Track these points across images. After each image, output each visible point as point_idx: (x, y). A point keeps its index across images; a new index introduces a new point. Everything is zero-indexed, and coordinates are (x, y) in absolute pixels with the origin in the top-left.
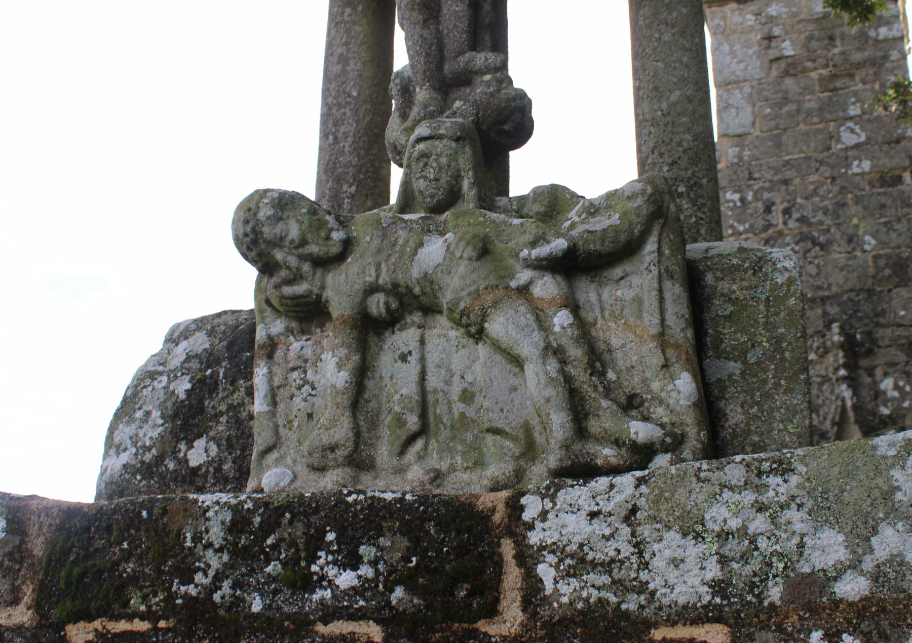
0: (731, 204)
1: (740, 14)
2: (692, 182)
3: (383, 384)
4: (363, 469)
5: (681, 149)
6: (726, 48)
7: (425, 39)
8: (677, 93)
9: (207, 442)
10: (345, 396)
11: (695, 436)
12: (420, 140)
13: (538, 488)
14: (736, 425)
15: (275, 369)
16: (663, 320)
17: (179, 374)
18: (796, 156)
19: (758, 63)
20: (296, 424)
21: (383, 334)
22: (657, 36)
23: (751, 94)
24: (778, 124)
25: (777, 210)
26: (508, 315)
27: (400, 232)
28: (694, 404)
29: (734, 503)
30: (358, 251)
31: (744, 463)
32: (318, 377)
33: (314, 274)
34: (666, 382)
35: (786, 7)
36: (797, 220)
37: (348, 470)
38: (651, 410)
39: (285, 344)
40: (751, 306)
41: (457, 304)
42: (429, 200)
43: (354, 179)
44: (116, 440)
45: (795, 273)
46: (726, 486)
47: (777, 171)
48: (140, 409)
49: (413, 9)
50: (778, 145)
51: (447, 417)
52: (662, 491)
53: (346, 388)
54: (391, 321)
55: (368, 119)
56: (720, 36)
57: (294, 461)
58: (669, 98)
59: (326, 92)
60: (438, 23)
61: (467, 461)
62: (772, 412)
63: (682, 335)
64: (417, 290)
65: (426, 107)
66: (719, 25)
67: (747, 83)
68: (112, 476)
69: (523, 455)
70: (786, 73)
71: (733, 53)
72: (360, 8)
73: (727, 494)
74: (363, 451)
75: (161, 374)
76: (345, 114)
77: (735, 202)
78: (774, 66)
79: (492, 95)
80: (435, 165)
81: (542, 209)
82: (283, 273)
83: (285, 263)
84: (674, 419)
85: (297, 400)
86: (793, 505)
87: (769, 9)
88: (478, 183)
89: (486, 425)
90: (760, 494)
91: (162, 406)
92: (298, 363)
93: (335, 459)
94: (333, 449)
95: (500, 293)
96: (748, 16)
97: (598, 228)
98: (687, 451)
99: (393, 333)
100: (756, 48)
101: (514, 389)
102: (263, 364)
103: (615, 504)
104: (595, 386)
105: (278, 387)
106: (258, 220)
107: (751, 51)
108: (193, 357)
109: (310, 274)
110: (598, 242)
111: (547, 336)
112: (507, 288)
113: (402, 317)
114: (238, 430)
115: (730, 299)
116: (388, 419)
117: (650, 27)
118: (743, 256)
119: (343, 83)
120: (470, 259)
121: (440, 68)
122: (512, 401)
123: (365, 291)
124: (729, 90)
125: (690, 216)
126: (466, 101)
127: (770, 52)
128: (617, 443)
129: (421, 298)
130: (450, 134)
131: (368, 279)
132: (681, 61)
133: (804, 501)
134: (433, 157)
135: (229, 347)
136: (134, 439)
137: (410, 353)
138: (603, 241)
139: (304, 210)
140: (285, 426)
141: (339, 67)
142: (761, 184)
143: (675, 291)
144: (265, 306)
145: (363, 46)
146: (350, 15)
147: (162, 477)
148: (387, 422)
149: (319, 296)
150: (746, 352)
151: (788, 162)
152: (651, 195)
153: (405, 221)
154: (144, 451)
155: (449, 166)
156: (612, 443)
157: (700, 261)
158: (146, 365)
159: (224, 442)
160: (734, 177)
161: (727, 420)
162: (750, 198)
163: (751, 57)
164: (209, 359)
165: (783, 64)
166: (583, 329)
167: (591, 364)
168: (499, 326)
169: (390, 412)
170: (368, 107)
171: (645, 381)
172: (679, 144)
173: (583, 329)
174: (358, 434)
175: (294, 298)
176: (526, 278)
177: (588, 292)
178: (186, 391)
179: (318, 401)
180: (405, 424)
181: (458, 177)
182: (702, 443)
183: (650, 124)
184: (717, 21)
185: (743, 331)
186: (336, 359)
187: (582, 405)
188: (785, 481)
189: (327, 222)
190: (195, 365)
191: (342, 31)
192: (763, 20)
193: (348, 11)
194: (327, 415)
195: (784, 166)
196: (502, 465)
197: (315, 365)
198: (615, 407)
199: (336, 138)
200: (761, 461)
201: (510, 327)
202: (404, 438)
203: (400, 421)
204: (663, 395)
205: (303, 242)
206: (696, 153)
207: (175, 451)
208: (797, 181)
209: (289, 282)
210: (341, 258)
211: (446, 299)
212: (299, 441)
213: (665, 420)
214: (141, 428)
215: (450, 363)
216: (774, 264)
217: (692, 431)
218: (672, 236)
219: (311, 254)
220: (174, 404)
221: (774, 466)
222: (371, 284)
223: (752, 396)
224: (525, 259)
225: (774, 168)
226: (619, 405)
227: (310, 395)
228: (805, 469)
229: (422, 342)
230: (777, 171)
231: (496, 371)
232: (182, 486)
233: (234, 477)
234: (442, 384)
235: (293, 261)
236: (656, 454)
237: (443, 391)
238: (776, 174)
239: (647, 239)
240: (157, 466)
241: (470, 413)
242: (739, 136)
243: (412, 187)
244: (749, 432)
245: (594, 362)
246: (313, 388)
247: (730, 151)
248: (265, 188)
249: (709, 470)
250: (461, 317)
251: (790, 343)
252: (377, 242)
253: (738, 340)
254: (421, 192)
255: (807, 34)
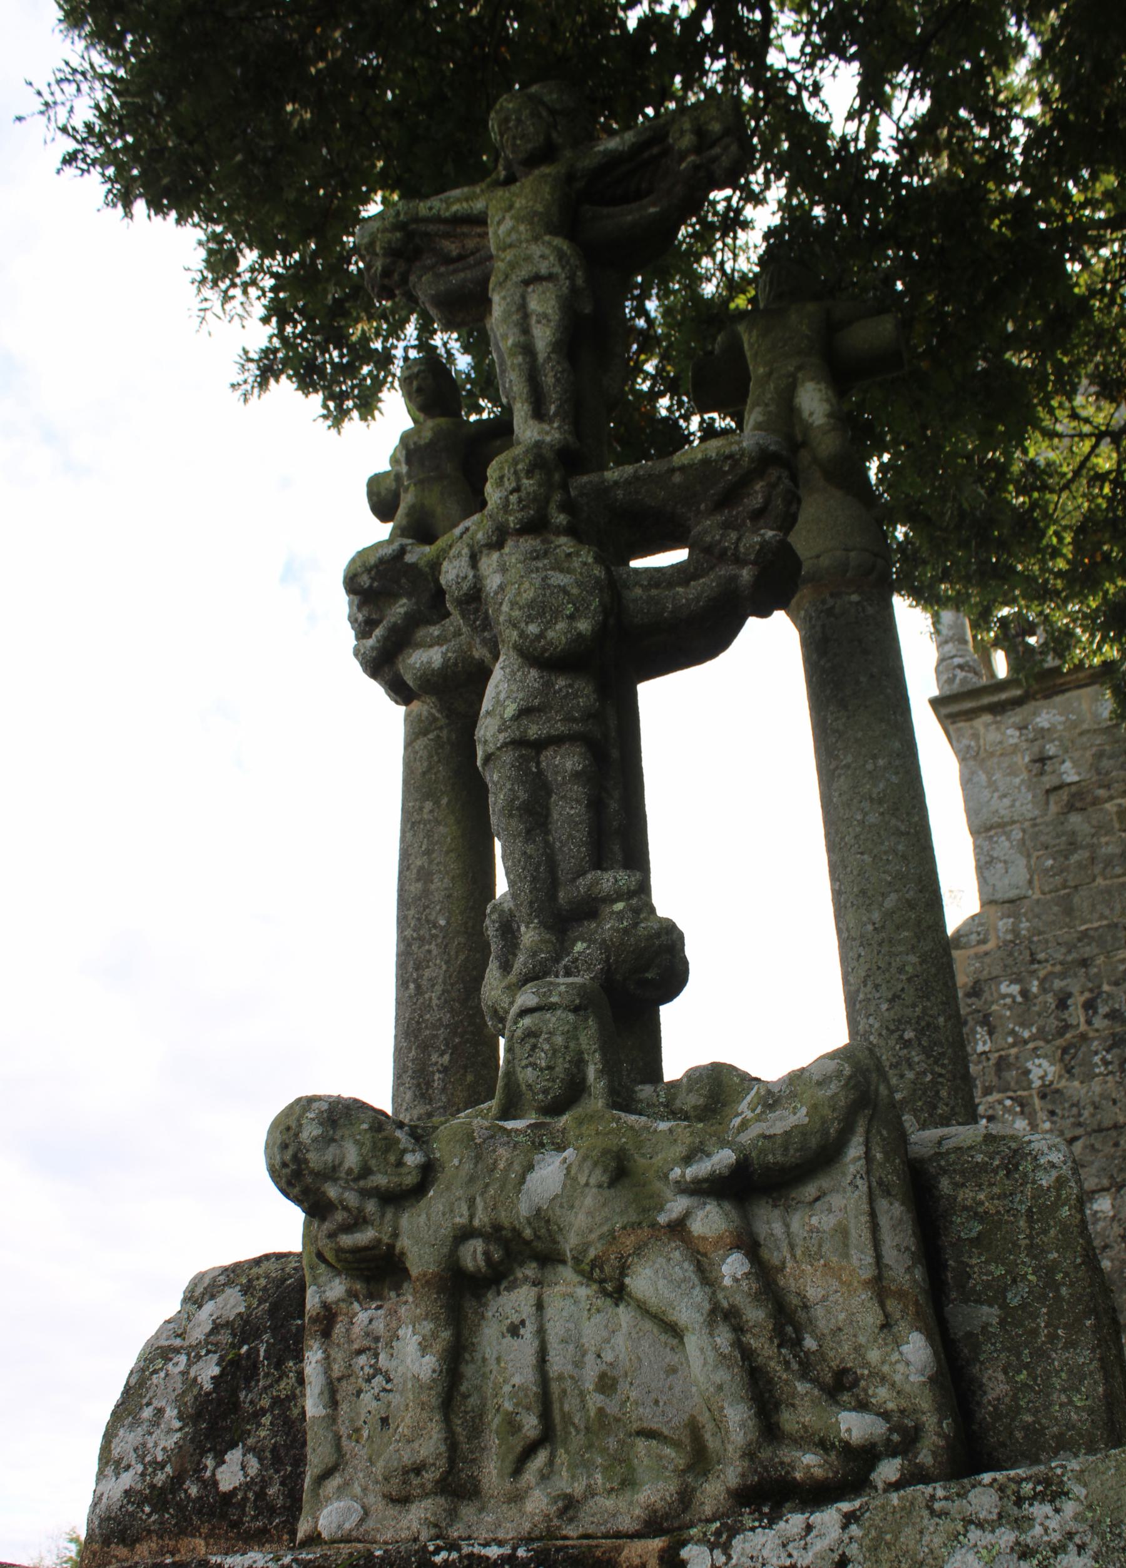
0: (1008, 1001)
1: (998, 729)
2: (923, 1023)
3: (487, 1370)
4: (464, 1498)
5: (904, 977)
6: (983, 778)
7: (530, 857)
8: (894, 896)
9: (244, 1455)
10: (433, 1392)
11: (935, 1431)
12: (524, 1012)
13: (705, 1534)
14: (998, 1399)
15: (333, 1352)
16: (878, 1257)
17: (203, 1352)
18: (1096, 925)
19: (1030, 797)
20: (365, 1434)
21: (485, 1295)
22: (859, 817)
23: (1023, 839)
24: (1066, 881)
25: (1075, 1004)
26: (657, 1266)
27: (501, 1151)
28: (931, 1379)
29: (986, 1547)
30: (443, 1178)
31: (996, 1485)
32: (394, 1363)
33: (383, 1216)
34: (889, 1349)
35: (1061, 714)
36: (1106, 1016)
37: (441, 1500)
38: (870, 1392)
39: (346, 1314)
40: (1007, 1222)
41: (585, 1251)
42: (541, 1096)
43: (447, 1045)
44: (115, 1453)
45: (1066, 1170)
46: (971, 1522)
47: (1071, 948)
48: (148, 1404)
49: (511, 816)
50: (1069, 911)
51: (578, 1415)
52: (881, 1533)
53: (433, 1380)
54: (496, 1277)
55: (462, 957)
56: (972, 763)
57: (365, 1490)
58: (882, 905)
59: (402, 921)
60: (547, 832)
61: (610, 1479)
62: (1049, 1378)
63: (907, 1277)
64: (528, 1233)
65: (534, 954)
66: (969, 747)
67: (1018, 825)
68: (108, 1508)
69: (690, 1468)
70: (1070, 808)
71: (992, 785)
72: (444, 801)
73: (974, 1534)
74: (462, 1470)
75: (177, 1351)
76: (429, 951)
77: (1013, 997)
78: (1053, 798)
79: (626, 931)
80: (546, 1047)
81: (701, 1101)
82: (340, 1216)
83: (341, 1202)
84: (904, 1404)
85: (366, 1397)
86: (1072, 1548)
87: (1038, 720)
88: (609, 1069)
89: (635, 1426)
90: (1023, 1531)
91: (179, 1400)
92: (366, 1343)
93: (422, 1485)
94: (418, 1469)
95: (646, 1231)
96: (1009, 732)
97: (778, 1129)
98: (924, 1451)
99: (499, 1294)
100: (1024, 775)
101: (672, 1370)
102: (316, 1346)
103: (815, 1555)
104: (787, 1363)
105: (339, 1379)
106: (300, 1143)
107: (1017, 781)
108: (222, 1326)
109: (377, 1217)
110: (779, 1152)
111: (714, 1293)
112: (654, 1225)
113: (510, 1271)
114: (287, 1435)
115: (976, 1213)
116: (497, 1421)
117: (849, 805)
118: (992, 1149)
119: (426, 907)
120: (600, 1186)
121: (552, 896)
122: (670, 1389)
123: (455, 1237)
124: (991, 837)
125: (924, 1073)
126: (590, 941)
127: (1045, 779)
128: (823, 1445)
129: (535, 1244)
130: (565, 1002)
131: (458, 1220)
132: (895, 852)
133: (1087, 1539)
134: (544, 1036)
135: (272, 1312)
136: (141, 1451)
137: (523, 1323)
138: (786, 1149)
139: (365, 1126)
140: (350, 1437)
141: (419, 885)
142: (1049, 968)
143: (892, 1211)
144: (315, 1260)
145: (452, 855)
146: (431, 811)
147: (181, 1507)
148: (494, 1426)
149: (391, 1247)
150: (1005, 1290)
151: (1085, 934)
152: (850, 1078)
153: (508, 1132)
154: (155, 1470)
155: (566, 1047)
156: (816, 1445)
157: (930, 1159)
158: (157, 1336)
159: (268, 1454)
160: (1010, 961)
161: (985, 1393)
162: (1035, 990)
163: (1019, 788)
164: (243, 1329)
165: (1064, 795)
166: (765, 1277)
167: (778, 1332)
168: (643, 1281)
169: (498, 1410)
170: (462, 940)
171: (858, 1348)
172: (901, 970)
173: (765, 1277)
174: (452, 1445)
175: (356, 1250)
176: (680, 1209)
177: (770, 1223)
178: (212, 1378)
179: (395, 1399)
180: (520, 1428)
181: (579, 1063)
182: (946, 1437)
183: (858, 943)
184: (965, 742)
185: (999, 1260)
186: (417, 1338)
187: (770, 1391)
188: (1057, 1511)
189: (398, 1141)
190: (225, 1337)
191: (421, 835)
192: (1031, 736)
193: (429, 805)
194: (408, 1420)
195: (1080, 940)
196: (661, 1485)
197: (389, 1345)
198: (816, 1392)
199: (418, 987)
200: (1019, 1481)
201: (661, 1283)
202: (519, 1449)
203: (512, 1426)
204: (886, 1369)
205: (366, 1171)
206: (926, 982)
207: (199, 1469)
208: (1100, 960)
209: (347, 1228)
210: (419, 1190)
211: (570, 1243)
212: (370, 1460)
213: (891, 1406)
214: (151, 1434)
215: (580, 1336)
216: (1035, 1158)
217: (930, 1421)
218: (885, 1133)
219: (377, 1188)
220: (196, 1398)
221: (1039, 1488)
222: (463, 1226)
223: (1019, 1355)
224: (677, 1182)
225: (1066, 943)
226: (823, 1387)
227: (384, 1390)
228: (1084, 1492)
229: (540, 1306)
230: (1071, 948)
231: (645, 1344)
232: (209, 1521)
233: (283, 1506)
234: (570, 1367)
235: (352, 1198)
236: (879, 1460)
237: (572, 1377)
238: (1069, 952)
239: (848, 1141)
240: (173, 1492)
241: (612, 1409)
242: (1011, 901)
243: (517, 1079)
244: (1017, 1410)
245: (782, 1326)
246: (389, 1380)
247: (1001, 923)
248: (310, 1094)
249: (946, 1498)
250: (592, 1269)
251: (1066, 1274)
252: (468, 1166)
253: (992, 1273)
254: (529, 1086)
255: (1094, 749)
